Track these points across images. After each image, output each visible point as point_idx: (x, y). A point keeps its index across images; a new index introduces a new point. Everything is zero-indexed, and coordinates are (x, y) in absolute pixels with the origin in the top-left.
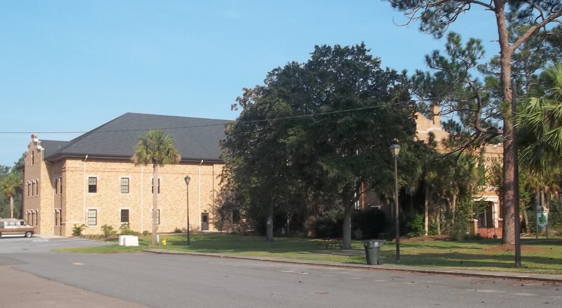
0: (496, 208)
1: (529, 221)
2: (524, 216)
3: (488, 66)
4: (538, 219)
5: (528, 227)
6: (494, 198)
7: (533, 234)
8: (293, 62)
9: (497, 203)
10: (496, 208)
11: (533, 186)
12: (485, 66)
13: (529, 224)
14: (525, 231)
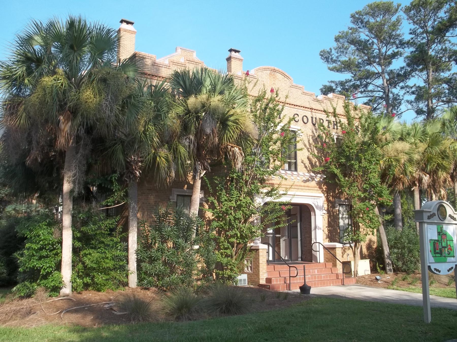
0: (320, 220)
1: (391, 248)
2: (379, 237)
3: (333, 52)
4: (428, 247)
5: (388, 261)
6: (316, 198)
7: (400, 275)
8: (72, 24)
9: (321, 208)
10: (320, 220)
11: (397, 171)
12: (329, 53)
13: (390, 254)
14: (384, 269)
